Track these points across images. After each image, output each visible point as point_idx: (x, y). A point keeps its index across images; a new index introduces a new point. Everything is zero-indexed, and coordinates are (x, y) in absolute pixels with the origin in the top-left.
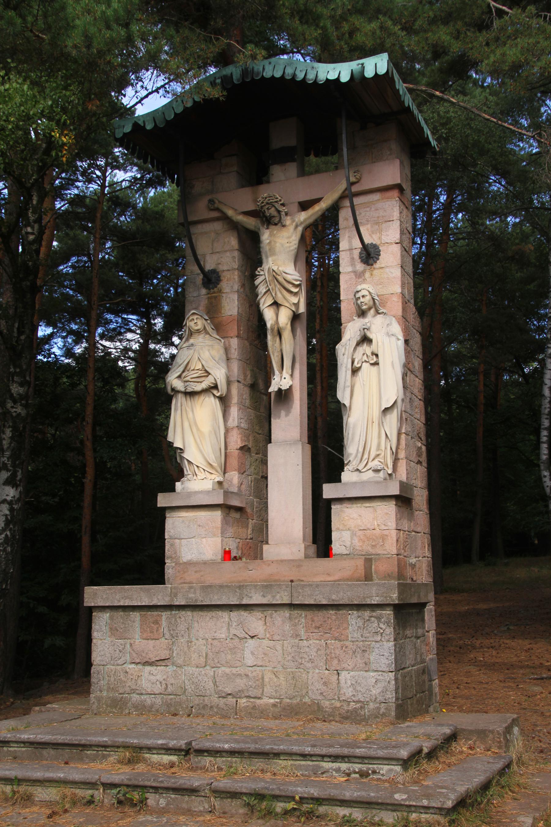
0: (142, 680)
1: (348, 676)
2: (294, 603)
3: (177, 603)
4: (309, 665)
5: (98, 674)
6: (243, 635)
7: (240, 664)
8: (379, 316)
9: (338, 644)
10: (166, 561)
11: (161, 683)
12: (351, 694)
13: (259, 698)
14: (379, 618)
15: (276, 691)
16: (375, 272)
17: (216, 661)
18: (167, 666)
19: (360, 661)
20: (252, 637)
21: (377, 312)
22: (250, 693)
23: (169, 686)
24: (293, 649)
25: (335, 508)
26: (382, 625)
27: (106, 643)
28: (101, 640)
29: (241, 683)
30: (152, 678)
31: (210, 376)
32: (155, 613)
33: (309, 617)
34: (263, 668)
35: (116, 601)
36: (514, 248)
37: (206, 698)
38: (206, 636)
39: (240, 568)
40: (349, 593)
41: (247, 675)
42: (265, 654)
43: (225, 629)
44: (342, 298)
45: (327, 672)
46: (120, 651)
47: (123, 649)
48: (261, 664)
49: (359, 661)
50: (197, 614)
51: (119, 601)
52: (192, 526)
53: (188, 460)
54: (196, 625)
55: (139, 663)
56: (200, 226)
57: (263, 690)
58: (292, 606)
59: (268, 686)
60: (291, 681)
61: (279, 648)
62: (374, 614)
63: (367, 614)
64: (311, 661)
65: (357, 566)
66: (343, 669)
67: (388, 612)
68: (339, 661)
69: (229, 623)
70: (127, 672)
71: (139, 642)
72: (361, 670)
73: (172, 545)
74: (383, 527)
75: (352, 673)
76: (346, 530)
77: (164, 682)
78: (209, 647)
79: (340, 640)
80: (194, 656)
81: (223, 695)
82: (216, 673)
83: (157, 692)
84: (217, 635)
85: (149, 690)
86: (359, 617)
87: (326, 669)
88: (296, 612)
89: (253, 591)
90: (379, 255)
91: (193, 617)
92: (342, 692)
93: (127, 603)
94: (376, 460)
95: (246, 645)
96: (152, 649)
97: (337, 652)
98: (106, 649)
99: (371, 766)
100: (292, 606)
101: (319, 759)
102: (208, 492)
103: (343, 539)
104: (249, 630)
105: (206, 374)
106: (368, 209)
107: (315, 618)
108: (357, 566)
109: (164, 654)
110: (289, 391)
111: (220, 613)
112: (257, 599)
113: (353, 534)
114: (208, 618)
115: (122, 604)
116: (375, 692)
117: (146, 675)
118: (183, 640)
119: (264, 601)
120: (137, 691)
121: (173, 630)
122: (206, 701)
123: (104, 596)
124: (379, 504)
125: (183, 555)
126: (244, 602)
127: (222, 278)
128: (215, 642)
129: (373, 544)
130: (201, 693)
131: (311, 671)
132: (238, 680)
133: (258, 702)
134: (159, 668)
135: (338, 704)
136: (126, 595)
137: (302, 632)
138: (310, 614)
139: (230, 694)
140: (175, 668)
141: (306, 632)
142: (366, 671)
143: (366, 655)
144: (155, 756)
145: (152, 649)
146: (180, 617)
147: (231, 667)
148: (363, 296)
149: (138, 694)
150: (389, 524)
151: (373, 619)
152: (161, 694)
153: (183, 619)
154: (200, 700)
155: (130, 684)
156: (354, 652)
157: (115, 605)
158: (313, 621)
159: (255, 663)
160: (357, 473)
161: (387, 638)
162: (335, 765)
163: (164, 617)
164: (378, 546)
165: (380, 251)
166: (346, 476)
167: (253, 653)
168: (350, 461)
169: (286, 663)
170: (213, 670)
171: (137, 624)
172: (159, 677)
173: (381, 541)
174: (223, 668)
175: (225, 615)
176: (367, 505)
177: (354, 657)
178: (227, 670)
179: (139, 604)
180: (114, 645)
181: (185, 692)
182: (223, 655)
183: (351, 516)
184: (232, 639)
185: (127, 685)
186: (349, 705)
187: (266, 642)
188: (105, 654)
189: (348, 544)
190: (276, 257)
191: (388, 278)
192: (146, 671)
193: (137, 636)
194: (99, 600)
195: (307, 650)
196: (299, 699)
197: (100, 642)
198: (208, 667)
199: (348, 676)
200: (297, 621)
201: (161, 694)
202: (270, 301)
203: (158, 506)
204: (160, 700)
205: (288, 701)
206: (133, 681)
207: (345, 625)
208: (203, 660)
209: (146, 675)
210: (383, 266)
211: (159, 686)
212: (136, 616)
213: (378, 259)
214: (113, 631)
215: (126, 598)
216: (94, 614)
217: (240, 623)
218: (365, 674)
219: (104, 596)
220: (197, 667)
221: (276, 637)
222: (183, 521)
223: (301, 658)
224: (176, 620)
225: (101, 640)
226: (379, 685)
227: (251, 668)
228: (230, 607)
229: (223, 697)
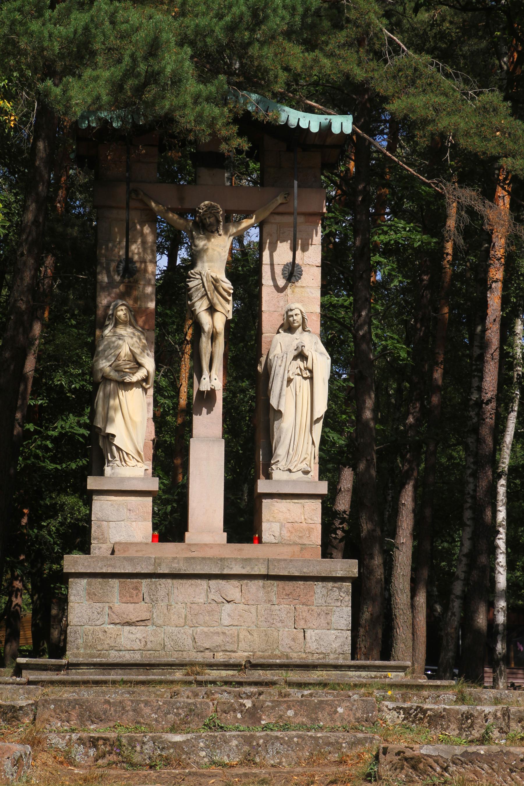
0: (121, 638)
1: (313, 634)
2: (270, 573)
3: (161, 572)
4: (280, 624)
5: (76, 633)
7: (217, 624)
8: (305, 333)
9: (306, 608)
10: (92, 541)
12: (315, 647)
13: (234, 652)
14: (340, 589)
15: (250, 646)
16: (297, 290)
17: (195, 621)
18: (147, 626)
19: (323, 621)
20: (228, 602)
21: (304, 330)
22: (227, 648)
23: (148, 643)
24: (266, 612)
25: (266, 502)
26: (342, 594)
27: (83, 606)
28: (78, 603)
29: (218, 640)
30: (131, 636)
32: (135, 580)
33: (281, 586)
34: (238, 628)
35: (98, 569)
36: (26, 132)
37: (184, 653)
38: (186, 600)
39: (183, 550)
40: (318, 567)
41: (224, 633)
42: (240, 616)
43: (203, 595)
44: (263, 309)
46: (98, 613)
47: (102, 611)
48: (237, 624)
49: (323, 621)
50: (177, 582)
51: (102, 569)
52: (121, 509)
54: (176, 591)
57: (238, 646)
58: (267, 577)
59: (243, 642)
60: (264, 638)
61: (253, 610)
62: (336, 585)
63: (330, 584)
64: (282, 621)
65: (294, 552)
66: (309, 628)
67: (348, 584)
68: (306, 621)
71: (118, 606)
73: (99, 527)
75: (316, 631)
76: (276, 522)
78: (188, 610)
79: (307, 605)
80: (174, 617)
81: (202, 649)
82: (195, 632)
83: (136, 649)
84: (196, 600)
86: (323, 587)
88: (269, 582)
89: (233, 563)
90: (301, 275)
91: (173, 584)
92: (307, 646)
93: (110, 570)
94: (304, 462)
95: (223, 608)
96: (133, 611)
97: (304, 614)
98: (84, 611)
99: (383, 673)
100: (267, 577)
102: (142, 479)
107: (286, 588)
108: (294, 552)
110: (212, 393)
111: (199, 581)
112: (237, 570)
113: (282, 527)
114: (187, 586)
115: (104, 571)
116: (335, 645)
117: (126, 634)
118: (163, 605)
119: (244, 572)
120: (116, 648)
121: (153, 595)
122: (185, 655)
123: (86, 564)
124: (307, 501)
125: (111, 537)
126: (225, 572)
128: (194, 606)
130: (180, 649)
131: (281, 630)
132: (215, 638)
133: (233, 655)
134: (138, 627)
135: (304, 656)
136: (109, 563)
137: (274, 599)
138: (281, 583)
139: (207, 649)
140: (155, 627)
143: (329, 617)
144: (215, 671)
145: (133, 611)
147: (208, 626)
148: (296, 315)
149: (116, 650)
150: (316, 519)
151: (335, 589)
152: (140, 650)
153: (163, 586)
154: (178, 654)
155: (109, 642)
156: (319, 615)
157: (97, 571)
159: (231, 624)
160: (288, 472)
161: (346, 604)
162: (358, 673)
163: (144, 583)
164: (304, 537)
165: (302, 271)
166: (277, 474)
167: (229, 615)
168: (278, 461)
169: (259, 623)
170: (192, 629)
171: (116, 590)
172: (139, 636)
173: (307, 533)
174: (201, 628)
175: (203, 583)
176: (296, 501)
177: (318, 618)
178: (206, 629)
180: (92, 608)
181: (164, 648)
182: (201, 616)
183: (281, 510)
185: (106, 643)
186: (313, 656)
187: (242, 606)
188: (82, 616)
189: (277, 534)
190: (213, 264)
192: (125, 630)
193: (116, 600)
194: (80, 567)
195: (278, 612)
196: (270, 652)
197: (77, 605)
198: (187, 627)
199: (313, 634)
200: (269, 589)
201: (140, 650)
203: (88, 488)
204: (139, 655)
205: (261, 653)
206: (112, 639)
207: (312, 593)
208: (182, 621)
209: (126, 634)
210: (304, 285)
211: (139, 643)
212: (115, 583)
213: (300, 278)
214: (91, 595)
215: (110, 566)
216: (70, 580)
217: (219, 590)
218: (327, 632)
219: (86, 564)
220: (177, 626)
221: (250, 602)
222: (112, 505)
223: (273, 619)
224: (156, 586)
225: (78, 603)
226: (338, 640)
229: (202, 652)
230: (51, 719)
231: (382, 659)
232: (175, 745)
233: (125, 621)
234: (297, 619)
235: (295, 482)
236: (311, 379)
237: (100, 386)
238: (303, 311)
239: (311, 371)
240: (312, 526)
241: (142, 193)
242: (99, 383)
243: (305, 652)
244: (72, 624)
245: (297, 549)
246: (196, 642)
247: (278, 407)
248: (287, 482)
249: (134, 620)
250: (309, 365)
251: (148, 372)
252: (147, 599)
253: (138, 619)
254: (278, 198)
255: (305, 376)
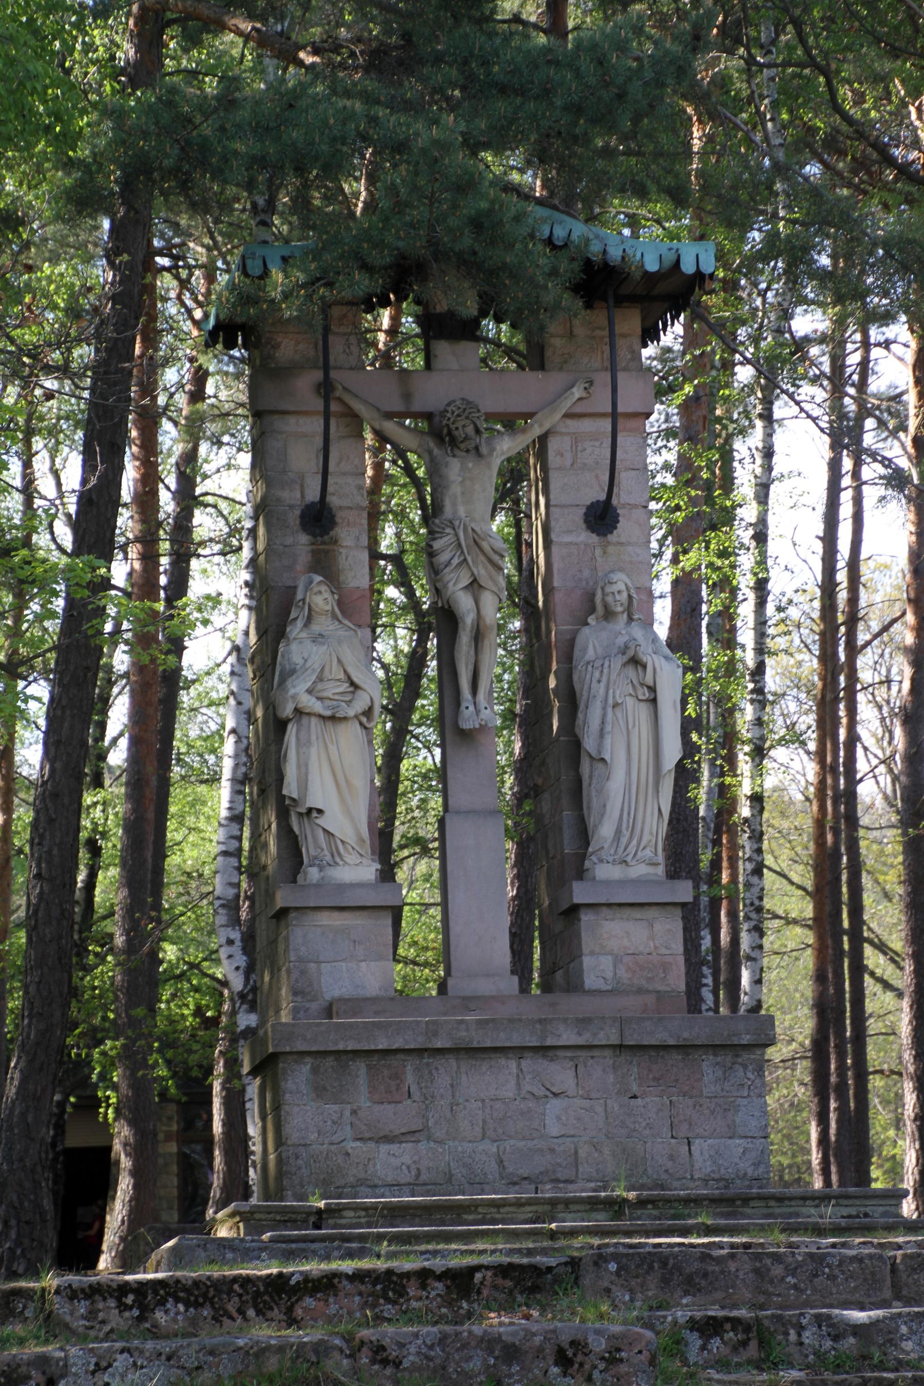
6: (542, 1092)
9: (690, 1102)
11: (408, 1167)
12: (709, 1169)
15: (598, 1171)
16: (611, 549)
17: (500, 1131)
18: (419, 1141)
20: (555, 1095)
22: (559, 1175)
25: (586, 918)
31: (359, 692)
34: (576, 1140)
40: (707, 1030)
41: (552, 1150)
43: (513, 1083)
45: (673, 1141)
46: (334, 1123)
53: (325, 830)
55: (370, 1139)
56: (292, 420)
57: (577, 1171)
58: (620, 1047)
61: (600, 1109)
68: (690, 1124)
69: (518, 1076)
70: (348, 1154)
71: (363, 1101)
72: (722, 1137)
74: (664, 951)
75: (710, 1141)
76: (606, 954)
77: (413, 1166)
78: (488, 1111)
79: (691, 1097)
81: (515, 1179)
82: (501, 1149)
83: (403, 1181)
85: (389, 1179)
86: (717, 1064)
87: (673, 1137)
95: (548, 1106)
101: (800, 1202)
103: (601, 967)
104: (553, 1085)
105: (351, 689)
106: (597, 444)
109: (416, 1125)
112: (568, 1037)
113: (617, 960)
119: (580, 1041)
125: (324, 990)
126: (549, 1042)
127: (338, 519)
128: (498, 1105)
129: (650, 975)
130: (477, 1180)
139: (525, 1179)
140: (432, 1144)
141: (640, 1085)
142: (730, 1138)
146: (437, 1069)
147: (524, 1138)
148: (619, 592)
149: (370, 1187)
150: (674, 946)
153: (442, 1070)
156: (713, 1112)
158: (650, 1070)
166: (605, 871)
167: (558, 1118)
172: (407, 1159)
174: (512, 1142)
176: (638, 916)
178: (521, 1144)
179: (373, 1047)
184: (524, 1098)
187: (578, 1102)
191: (631, 562)
199: (705, 1146)
202: (465, 581)
206: (361, 1167)
208: (478, 1130)
210: (623, 540)
212: (360, 1068)
213: (616, 528)
214: (319, 1091)
221: (593, 1095)
224: (430, 1073)
225: (298, 1105)
227: (556, 1140)
228: (520, 1051)
230: (613, 1287)
231: (857, 1185)
232: (858, 1330)
233: (382, 1134)
234: (675, 1121)
235: (638, 883)
236: (654, 701)
237: (290, 726)
238: (630, 585)
239: (653, 689)
240: (670, 959)
241: (340, 388)
242: (289, 720)
243: (692, 1178)
244: (289, 1142)
245: (650, 1000)
246: (504, 1167)
247: (600, 753)
248: (623, 883)
249: (397, 1132)
250: (649, 680)
251: (372, 700)
252: (416, 1096)
253: (403, 1130)
254: (575, 390)
255: (641, 697)
